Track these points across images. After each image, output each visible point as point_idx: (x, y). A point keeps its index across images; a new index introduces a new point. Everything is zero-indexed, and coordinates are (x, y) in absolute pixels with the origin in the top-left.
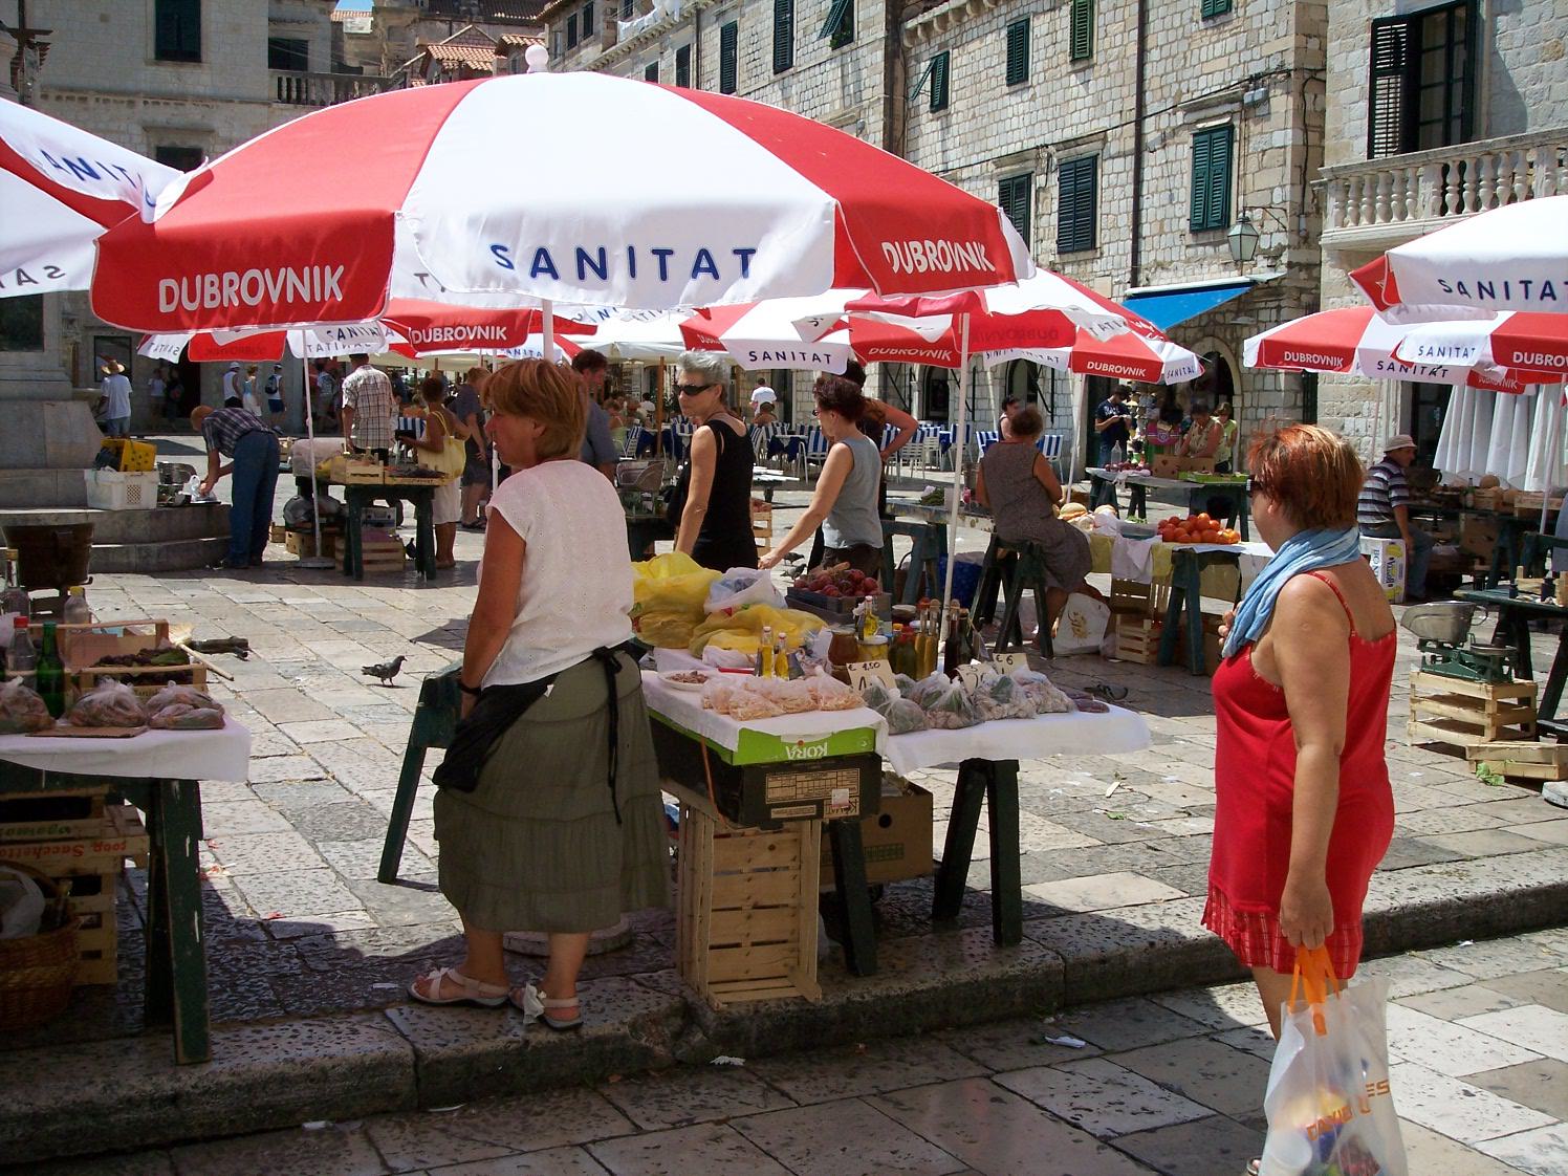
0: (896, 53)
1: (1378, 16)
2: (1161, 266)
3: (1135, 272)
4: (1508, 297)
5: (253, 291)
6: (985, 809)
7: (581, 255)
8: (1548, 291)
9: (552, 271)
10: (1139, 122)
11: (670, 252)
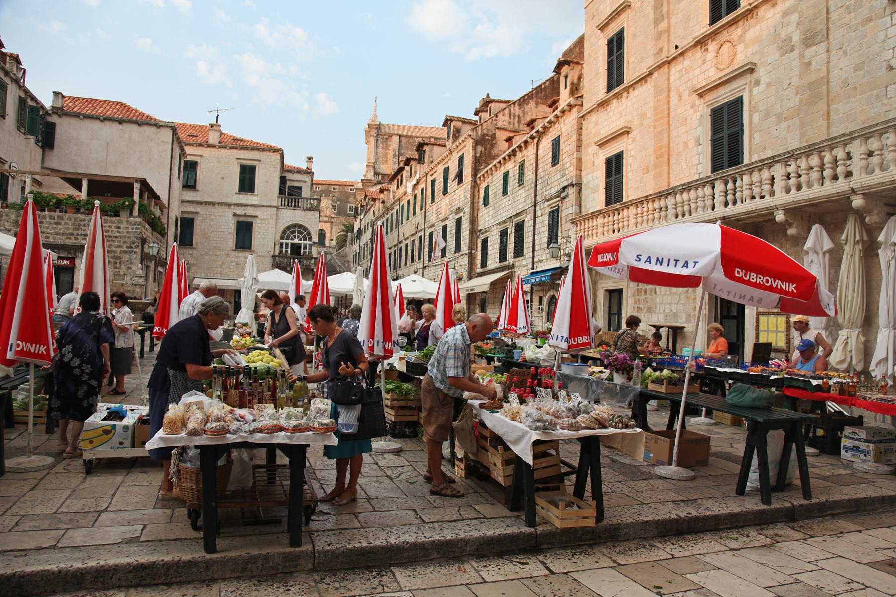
0: (475, 185)
1: (559, 165)
2: (540, 261)
3: (533, 264)
6: (589, 476)
7: (658, 259)
9: (650, 262)
10: (535, 206)
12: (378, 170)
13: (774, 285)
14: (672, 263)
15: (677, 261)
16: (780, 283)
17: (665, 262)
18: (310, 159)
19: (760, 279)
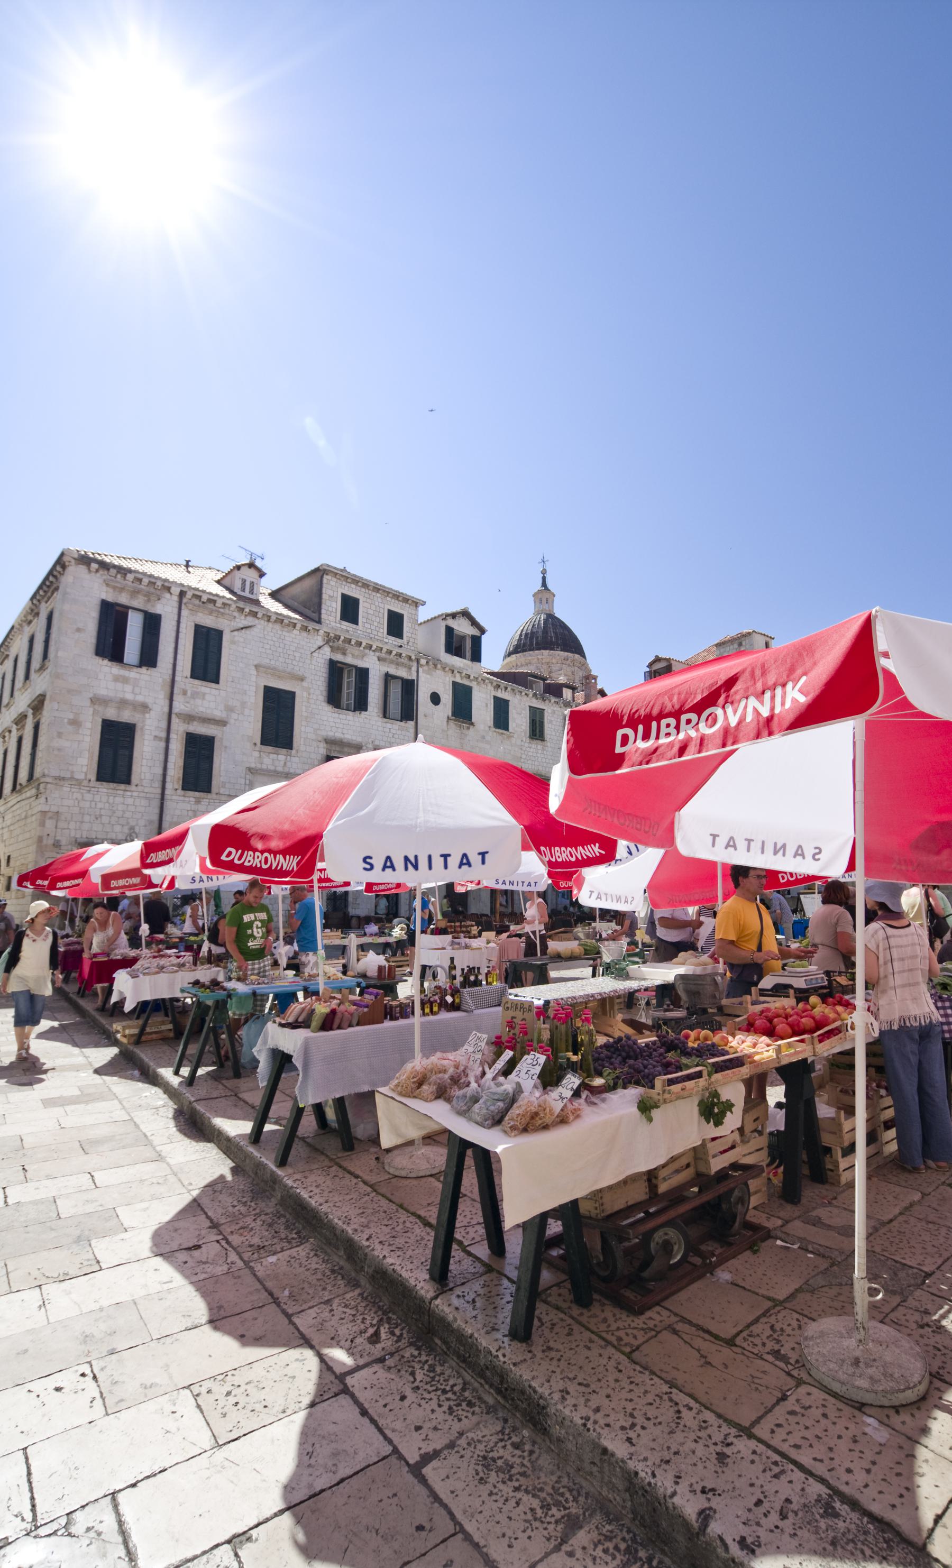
4: (430, 868)
5: (266, 863)
7: (406, 859)
8: (388, 864)
11: (449, 855)
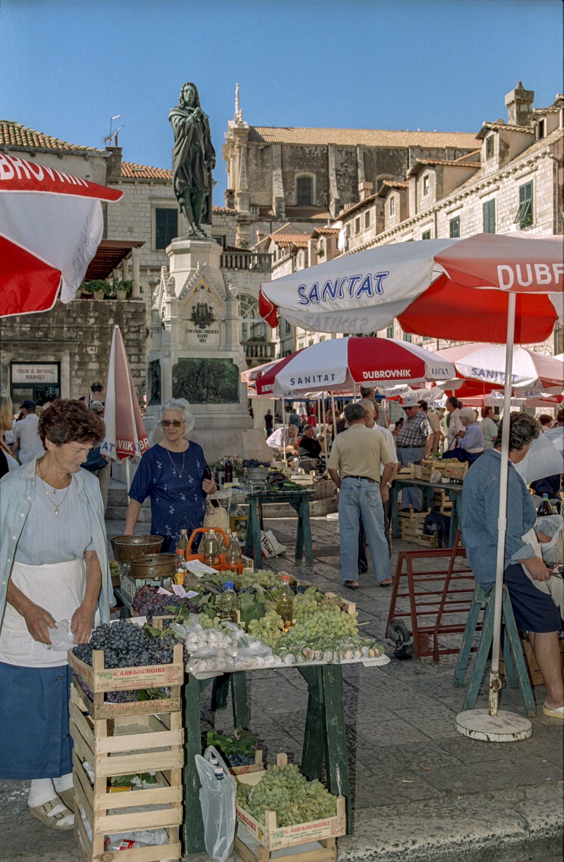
12: (253, 201)
13: (394, 376)
14: (317, 379)
15: (319, 376)
16: (398, 371)
17: (312, 380)
18: (55, 493)
19: (382, 374)
